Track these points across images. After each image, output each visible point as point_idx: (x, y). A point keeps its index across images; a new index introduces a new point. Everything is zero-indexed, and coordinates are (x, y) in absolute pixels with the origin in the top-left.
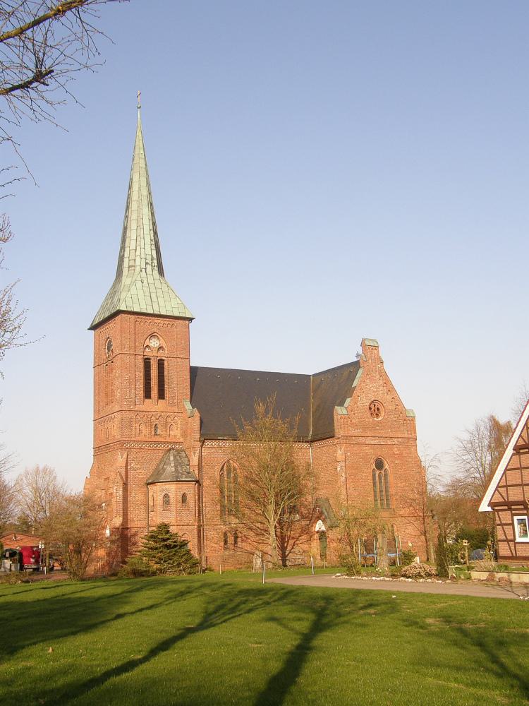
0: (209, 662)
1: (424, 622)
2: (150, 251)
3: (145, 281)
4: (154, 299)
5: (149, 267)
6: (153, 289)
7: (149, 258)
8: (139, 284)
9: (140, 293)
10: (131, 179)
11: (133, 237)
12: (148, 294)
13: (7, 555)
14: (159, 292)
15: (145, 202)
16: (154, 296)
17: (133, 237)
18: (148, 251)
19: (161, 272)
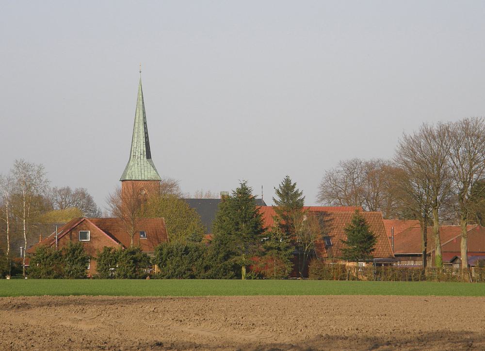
0: (50, 215)
1: (472, 256)
2: (143, 148)
3: (139, 163)
4: (143, 172)
5: (142, 156)
6: (142, 167)
7: (142, 151)
8: (136, 165)
9: (137, 170)
10: (118, 241)
11: (136, 141)
12: (140, 170)
13: (92, 268)
14: (145, 165)
15: (142, 123)
16: (143, 171)
17: (136, 141)
18: (142, 148)
19: (149, 156)
